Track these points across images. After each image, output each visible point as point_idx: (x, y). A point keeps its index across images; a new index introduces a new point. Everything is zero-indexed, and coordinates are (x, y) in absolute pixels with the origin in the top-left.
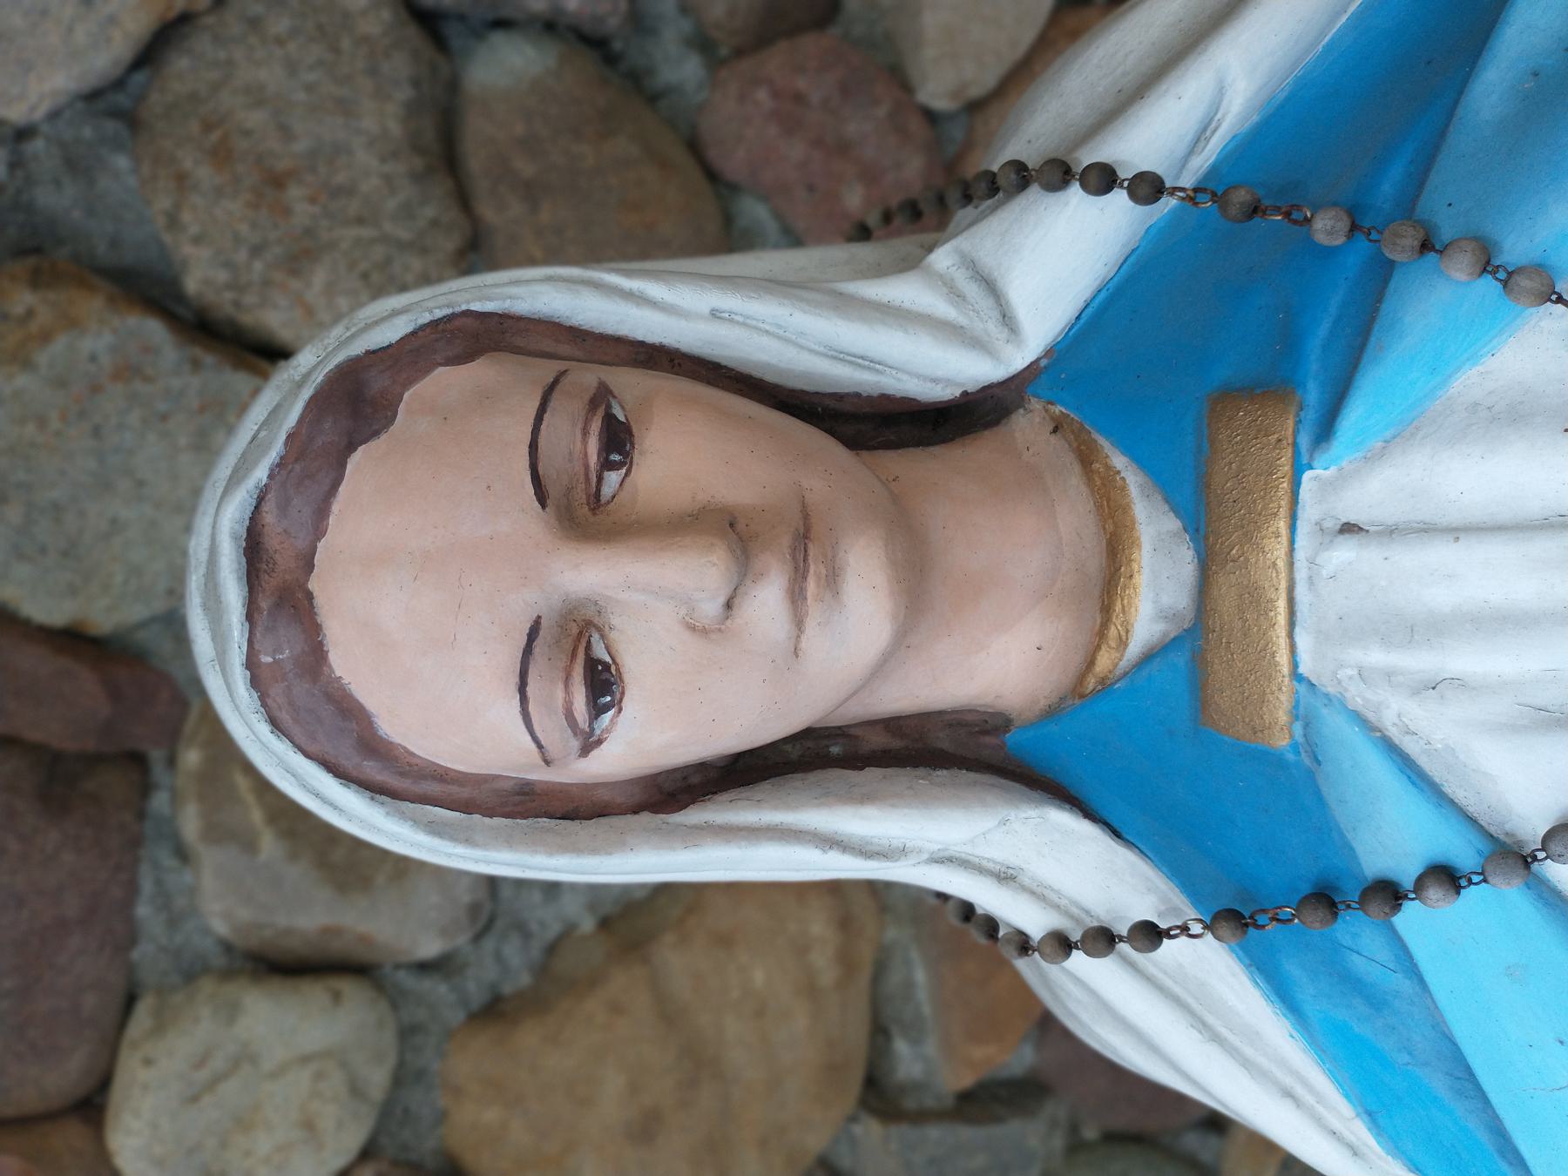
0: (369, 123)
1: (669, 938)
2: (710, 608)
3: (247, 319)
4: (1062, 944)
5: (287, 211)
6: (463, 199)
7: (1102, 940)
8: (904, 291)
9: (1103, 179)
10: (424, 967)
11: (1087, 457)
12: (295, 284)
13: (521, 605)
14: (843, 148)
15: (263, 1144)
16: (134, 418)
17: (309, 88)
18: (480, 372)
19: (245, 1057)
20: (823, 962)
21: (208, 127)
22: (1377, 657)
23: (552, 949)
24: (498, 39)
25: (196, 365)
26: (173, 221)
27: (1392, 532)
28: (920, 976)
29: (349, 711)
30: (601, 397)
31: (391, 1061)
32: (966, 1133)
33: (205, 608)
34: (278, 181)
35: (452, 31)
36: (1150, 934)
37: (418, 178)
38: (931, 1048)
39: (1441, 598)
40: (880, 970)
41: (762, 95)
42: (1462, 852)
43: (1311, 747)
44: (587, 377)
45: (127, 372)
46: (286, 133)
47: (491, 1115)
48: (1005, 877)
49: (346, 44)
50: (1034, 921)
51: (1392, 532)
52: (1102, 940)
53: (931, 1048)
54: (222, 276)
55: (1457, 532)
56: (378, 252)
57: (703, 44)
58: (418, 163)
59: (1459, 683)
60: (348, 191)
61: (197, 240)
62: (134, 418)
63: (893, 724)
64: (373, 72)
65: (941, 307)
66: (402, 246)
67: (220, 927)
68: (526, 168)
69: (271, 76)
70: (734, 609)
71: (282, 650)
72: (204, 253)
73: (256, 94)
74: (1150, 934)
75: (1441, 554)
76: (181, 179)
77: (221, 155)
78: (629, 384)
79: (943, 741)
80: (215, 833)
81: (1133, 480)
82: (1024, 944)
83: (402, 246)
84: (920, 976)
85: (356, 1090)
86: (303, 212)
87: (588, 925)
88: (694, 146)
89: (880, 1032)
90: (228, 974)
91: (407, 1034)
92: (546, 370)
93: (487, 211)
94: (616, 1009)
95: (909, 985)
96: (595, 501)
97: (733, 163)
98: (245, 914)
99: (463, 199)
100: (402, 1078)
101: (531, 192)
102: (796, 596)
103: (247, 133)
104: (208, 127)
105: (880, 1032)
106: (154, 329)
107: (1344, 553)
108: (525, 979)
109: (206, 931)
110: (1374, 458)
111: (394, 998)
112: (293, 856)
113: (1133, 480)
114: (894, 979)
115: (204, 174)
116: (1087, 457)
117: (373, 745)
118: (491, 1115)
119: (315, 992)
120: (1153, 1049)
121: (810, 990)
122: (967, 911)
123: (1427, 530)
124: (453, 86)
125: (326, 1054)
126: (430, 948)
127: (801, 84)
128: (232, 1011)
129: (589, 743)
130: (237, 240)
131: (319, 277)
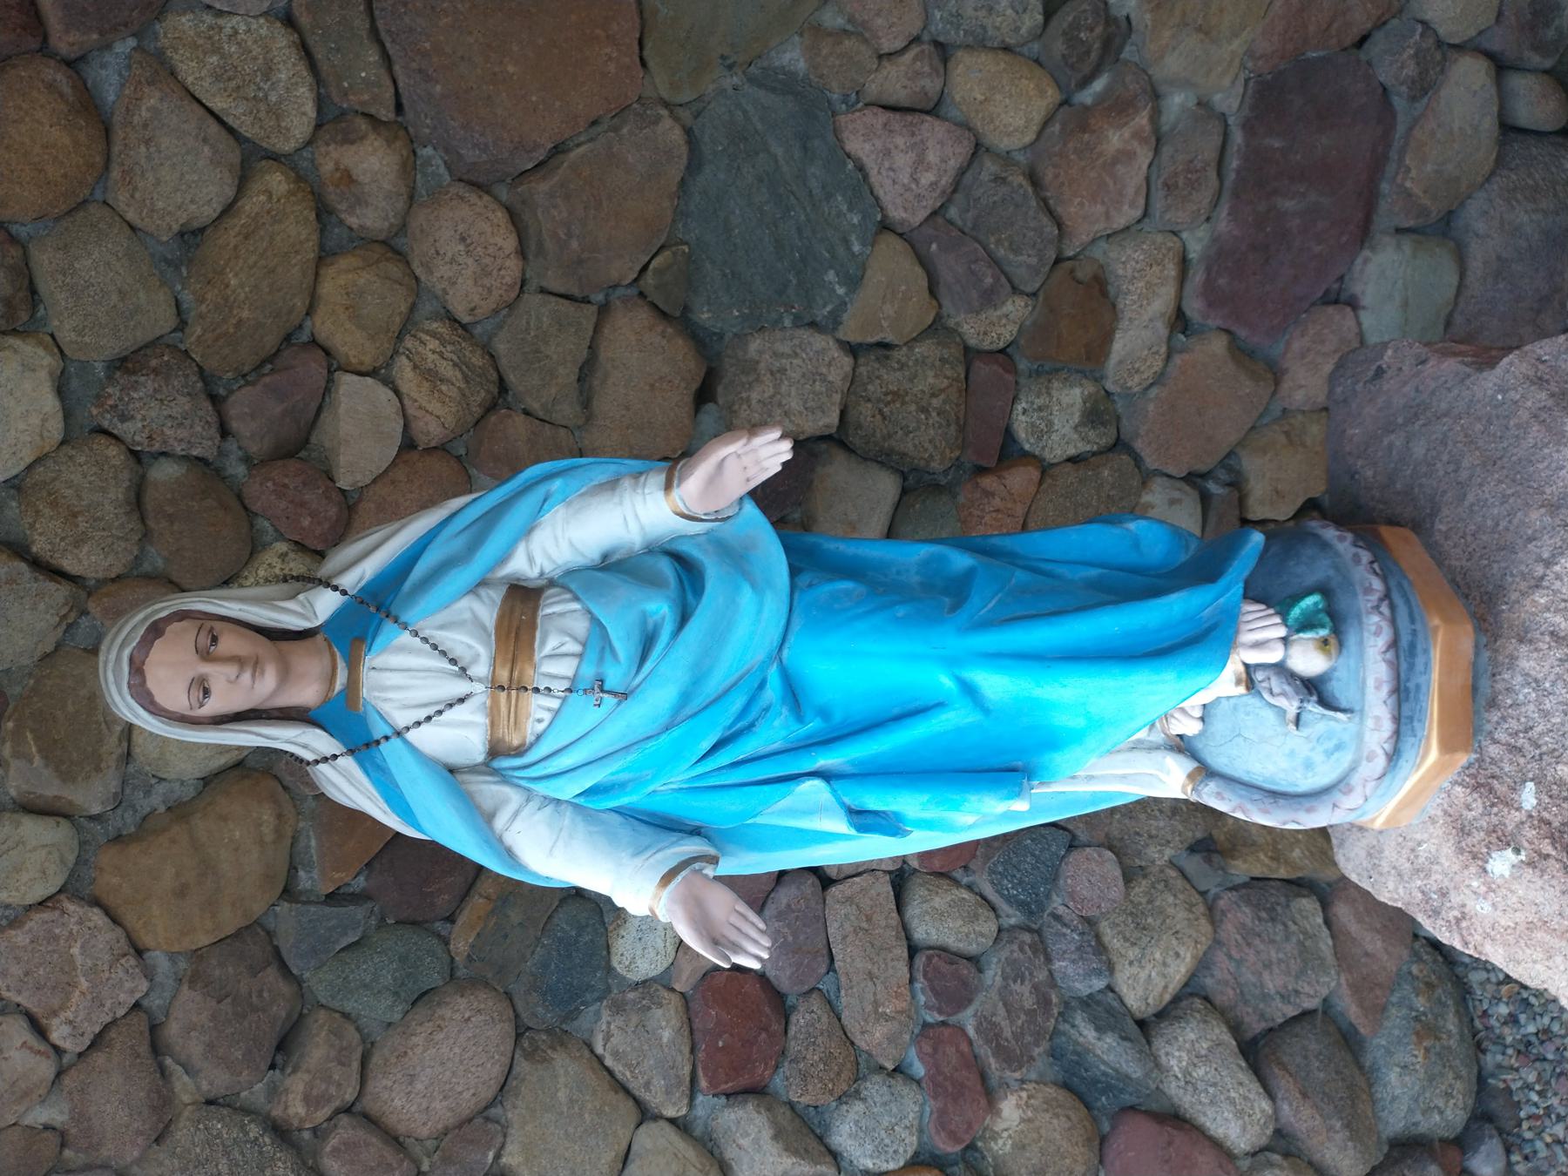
0: (112, 496)
1: (199, 815)
2: (233, 677)
3: (53, 562)
4: (317, 762)
5: (77, 526)
6: (143, 519)
7: (325, 760)
8: (290, 605)
9: (335, 588)
10: (92, 818)
11: (330, 647)
12: (76, 551)
13: (191, 674)
14: (302, 504)
15: (25, 877)
16: (11, 598)
17: (90, 483)
18: (184, 624)
19: (21, 842)
20: (268, 831)
21: (50, 494)
22: (377, 694)
23: (144, 819)
24: (162, 460)
25: (36, 580)
26: (32, 526)
27: (381, 669)
28: (313, 843)
29: (149, 694)
30: (211, 630)
31: (76, 853)
32: (327, 910)
33: (113, 671)
34: (75, 515)
35: (145, 460)
36: (335, 757)
37: (127, 514)
38: (315, 874)
39: (388, 683)
40: (295, 840)
41: (269, 484)
42: (389, 732)
43: (365, 712)
44: (208, 624)
45: (11, 581)
46: (80, 498)
47: (115, 880)
48: (305, 747)
49: (106, 467)
50: (309, 757)
51: (381, 669)
52: (325, 760)
53: (315, 874)
54: (49, 547)
55: (391, 670)
56: (110, 540)
57: (247, 460)
58: (128, 508)
59: (390, 700)
60: (101, 519)
61: (41, 534)
62: (11, 598)
63: (281, 709)
64: (115, 478)
65: (298, 608)
66: (119, 538)
67: (13, 793)
68: (170, 510)
69: (76, 478)
70: (638, 861)
71: (137, 681)
72: (43, 538)
73: (69, 484)
74: (335, 757)
75: (388, 674)
76: (37, 512)
77: (54, 505)
78: (218, 625)
79: (294, 715)
80: (17, 755)
81: (338, 654)
82: (308, 763)
83: (119, 538)
84: (313, 843)
85: (63, 861)
86: (83, 526)
87: (162, 809)
88: (239, 497)
89: (292, 869)
90: (14, 811)
91: (82, 844)
92: (199, 623)
93: (151, 523)
94: (173, 841)
95: (308, 847)
96: (208, 653)
97: (256, 507)
98: (25, 787)
99: (143, 519)
100: (80, 861)
101: (171, 519)
102: (253, 676)
103: (65, 497)
104: (50, 494)
105: (292, 869)
106: (23, 566)
107: (372, 673)
108: (133, 829)
109: (7, 794)
110: (378, 655)
111: (78, 829)
112: (47, 766)
113: (338, 654)
114: (302, 843)
115: (47, 511)
116: (330, 647)
117: (153, 702)
118: (115, 880)
119: (51, 821)
120: (339, 790)
121: (261, 842)
122: (292, 755)
123: (387, 670)
124: (143, 477)
125: (53, 845)
126: (96, 809)
127: (286, 481)
128: (18, 824)
129: (201, 705)
130: (56, 534)
131: (85, 549)
